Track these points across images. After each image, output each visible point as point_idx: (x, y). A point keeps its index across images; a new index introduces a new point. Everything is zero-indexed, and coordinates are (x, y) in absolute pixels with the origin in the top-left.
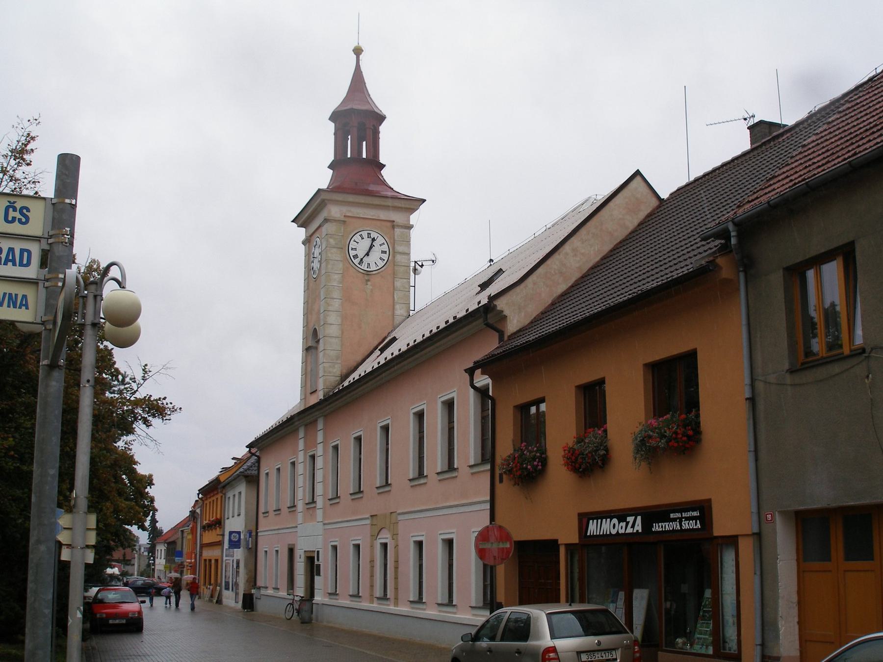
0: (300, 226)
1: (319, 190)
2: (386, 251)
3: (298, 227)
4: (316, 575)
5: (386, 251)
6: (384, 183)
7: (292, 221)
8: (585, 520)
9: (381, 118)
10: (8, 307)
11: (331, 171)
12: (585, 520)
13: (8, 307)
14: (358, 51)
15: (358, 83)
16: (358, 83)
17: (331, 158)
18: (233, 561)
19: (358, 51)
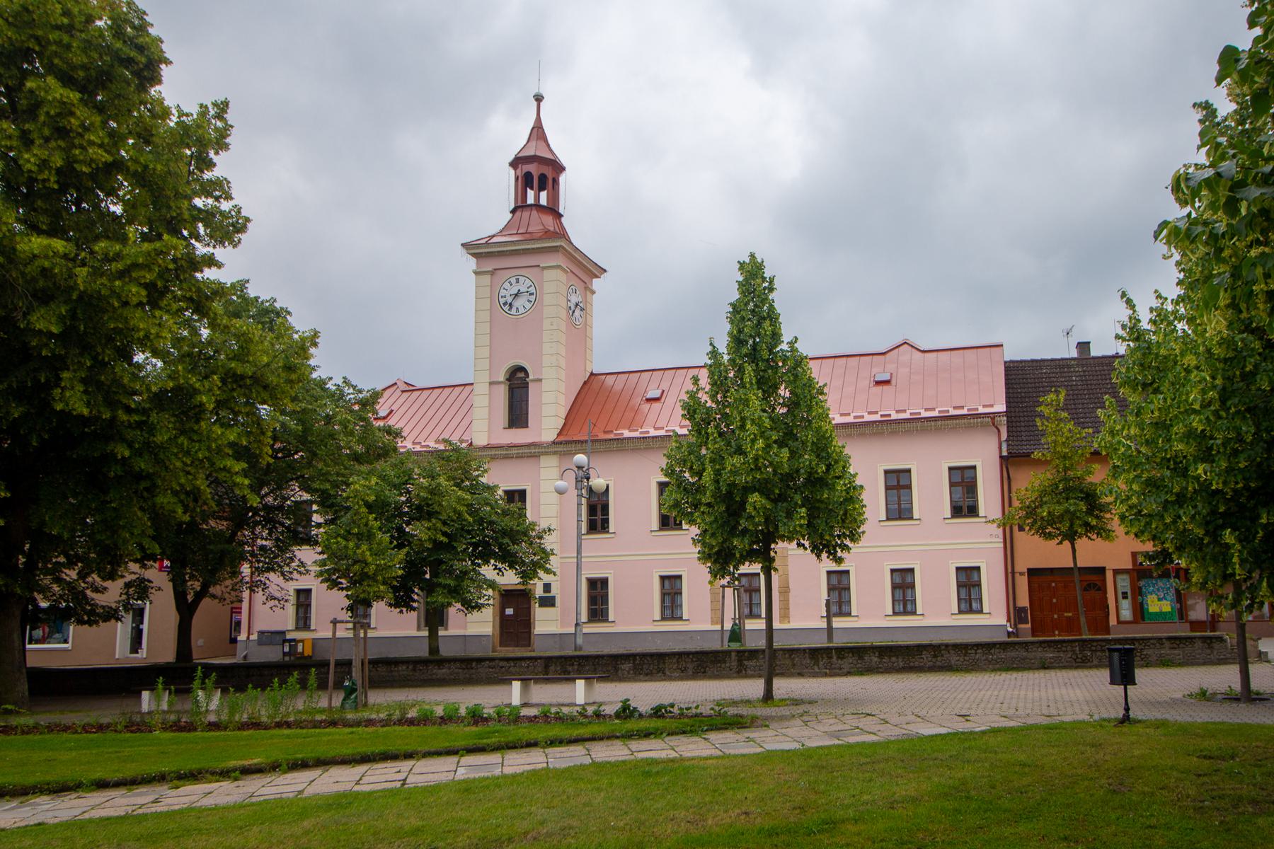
4: (550, 592)
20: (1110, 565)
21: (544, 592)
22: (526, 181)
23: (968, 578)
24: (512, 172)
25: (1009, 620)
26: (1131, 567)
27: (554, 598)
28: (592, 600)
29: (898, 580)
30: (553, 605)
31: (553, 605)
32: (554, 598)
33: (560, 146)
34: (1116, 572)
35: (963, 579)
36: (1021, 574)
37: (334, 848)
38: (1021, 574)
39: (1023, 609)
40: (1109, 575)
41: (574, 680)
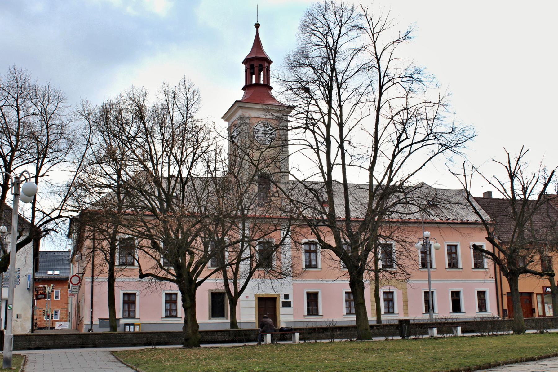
0: (226, 120)
1: (236, 101)
2: (317, 314)
3: (225, 121)
4: (288, 299)
5: (317, 314)
6: (273, 99)
7: (222, 118)
8: (545, 288)
9: (270, 62)
10: (316, 294)
11: (243, 92)
12: (545, 288)
13: (316, 294)
14: (257, 26)
15: (257, 41)
16: (257, 41)
17: (243, 84)
18: (52, 318)
19: (257, 26)
20: (536, 292)
21: (285, 299)
22: (250, 71)
23: (171, 298)
24: (244, 66)
25: (499, 314)
26: (542, 293)
27: (290, 302)
28: (427, 302)
29: (168, 299)
30: (290, 306)
31: (290, 306)
32: (290, 302)
33: (268, 50)
34: (537, 294)
35: (126, 299)
36: (504, 295)
37: (439, 371)
38: (504, 295)
39: (506, 310)
40: (535, 295)
41: (433, 328)
